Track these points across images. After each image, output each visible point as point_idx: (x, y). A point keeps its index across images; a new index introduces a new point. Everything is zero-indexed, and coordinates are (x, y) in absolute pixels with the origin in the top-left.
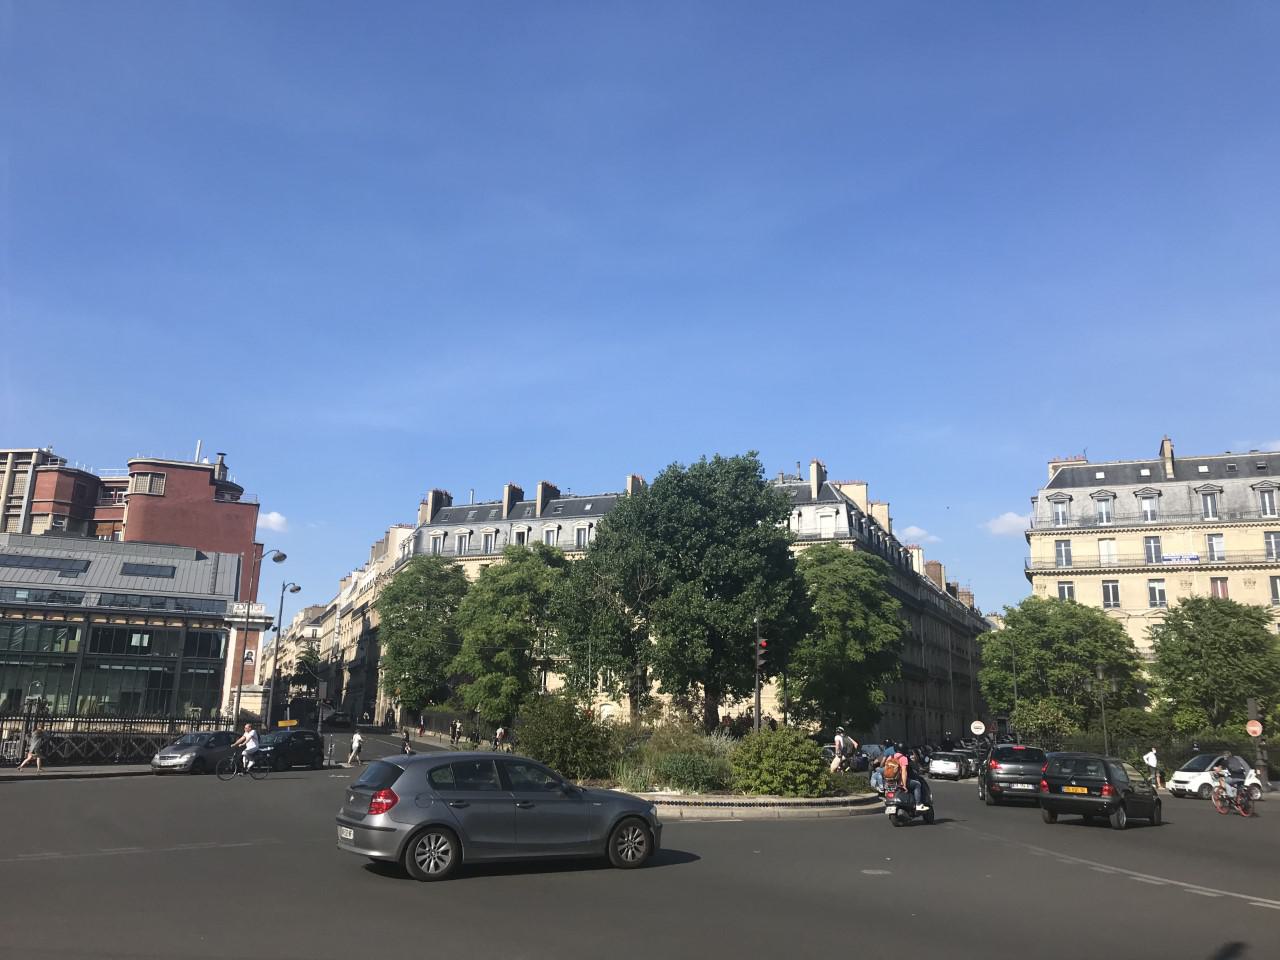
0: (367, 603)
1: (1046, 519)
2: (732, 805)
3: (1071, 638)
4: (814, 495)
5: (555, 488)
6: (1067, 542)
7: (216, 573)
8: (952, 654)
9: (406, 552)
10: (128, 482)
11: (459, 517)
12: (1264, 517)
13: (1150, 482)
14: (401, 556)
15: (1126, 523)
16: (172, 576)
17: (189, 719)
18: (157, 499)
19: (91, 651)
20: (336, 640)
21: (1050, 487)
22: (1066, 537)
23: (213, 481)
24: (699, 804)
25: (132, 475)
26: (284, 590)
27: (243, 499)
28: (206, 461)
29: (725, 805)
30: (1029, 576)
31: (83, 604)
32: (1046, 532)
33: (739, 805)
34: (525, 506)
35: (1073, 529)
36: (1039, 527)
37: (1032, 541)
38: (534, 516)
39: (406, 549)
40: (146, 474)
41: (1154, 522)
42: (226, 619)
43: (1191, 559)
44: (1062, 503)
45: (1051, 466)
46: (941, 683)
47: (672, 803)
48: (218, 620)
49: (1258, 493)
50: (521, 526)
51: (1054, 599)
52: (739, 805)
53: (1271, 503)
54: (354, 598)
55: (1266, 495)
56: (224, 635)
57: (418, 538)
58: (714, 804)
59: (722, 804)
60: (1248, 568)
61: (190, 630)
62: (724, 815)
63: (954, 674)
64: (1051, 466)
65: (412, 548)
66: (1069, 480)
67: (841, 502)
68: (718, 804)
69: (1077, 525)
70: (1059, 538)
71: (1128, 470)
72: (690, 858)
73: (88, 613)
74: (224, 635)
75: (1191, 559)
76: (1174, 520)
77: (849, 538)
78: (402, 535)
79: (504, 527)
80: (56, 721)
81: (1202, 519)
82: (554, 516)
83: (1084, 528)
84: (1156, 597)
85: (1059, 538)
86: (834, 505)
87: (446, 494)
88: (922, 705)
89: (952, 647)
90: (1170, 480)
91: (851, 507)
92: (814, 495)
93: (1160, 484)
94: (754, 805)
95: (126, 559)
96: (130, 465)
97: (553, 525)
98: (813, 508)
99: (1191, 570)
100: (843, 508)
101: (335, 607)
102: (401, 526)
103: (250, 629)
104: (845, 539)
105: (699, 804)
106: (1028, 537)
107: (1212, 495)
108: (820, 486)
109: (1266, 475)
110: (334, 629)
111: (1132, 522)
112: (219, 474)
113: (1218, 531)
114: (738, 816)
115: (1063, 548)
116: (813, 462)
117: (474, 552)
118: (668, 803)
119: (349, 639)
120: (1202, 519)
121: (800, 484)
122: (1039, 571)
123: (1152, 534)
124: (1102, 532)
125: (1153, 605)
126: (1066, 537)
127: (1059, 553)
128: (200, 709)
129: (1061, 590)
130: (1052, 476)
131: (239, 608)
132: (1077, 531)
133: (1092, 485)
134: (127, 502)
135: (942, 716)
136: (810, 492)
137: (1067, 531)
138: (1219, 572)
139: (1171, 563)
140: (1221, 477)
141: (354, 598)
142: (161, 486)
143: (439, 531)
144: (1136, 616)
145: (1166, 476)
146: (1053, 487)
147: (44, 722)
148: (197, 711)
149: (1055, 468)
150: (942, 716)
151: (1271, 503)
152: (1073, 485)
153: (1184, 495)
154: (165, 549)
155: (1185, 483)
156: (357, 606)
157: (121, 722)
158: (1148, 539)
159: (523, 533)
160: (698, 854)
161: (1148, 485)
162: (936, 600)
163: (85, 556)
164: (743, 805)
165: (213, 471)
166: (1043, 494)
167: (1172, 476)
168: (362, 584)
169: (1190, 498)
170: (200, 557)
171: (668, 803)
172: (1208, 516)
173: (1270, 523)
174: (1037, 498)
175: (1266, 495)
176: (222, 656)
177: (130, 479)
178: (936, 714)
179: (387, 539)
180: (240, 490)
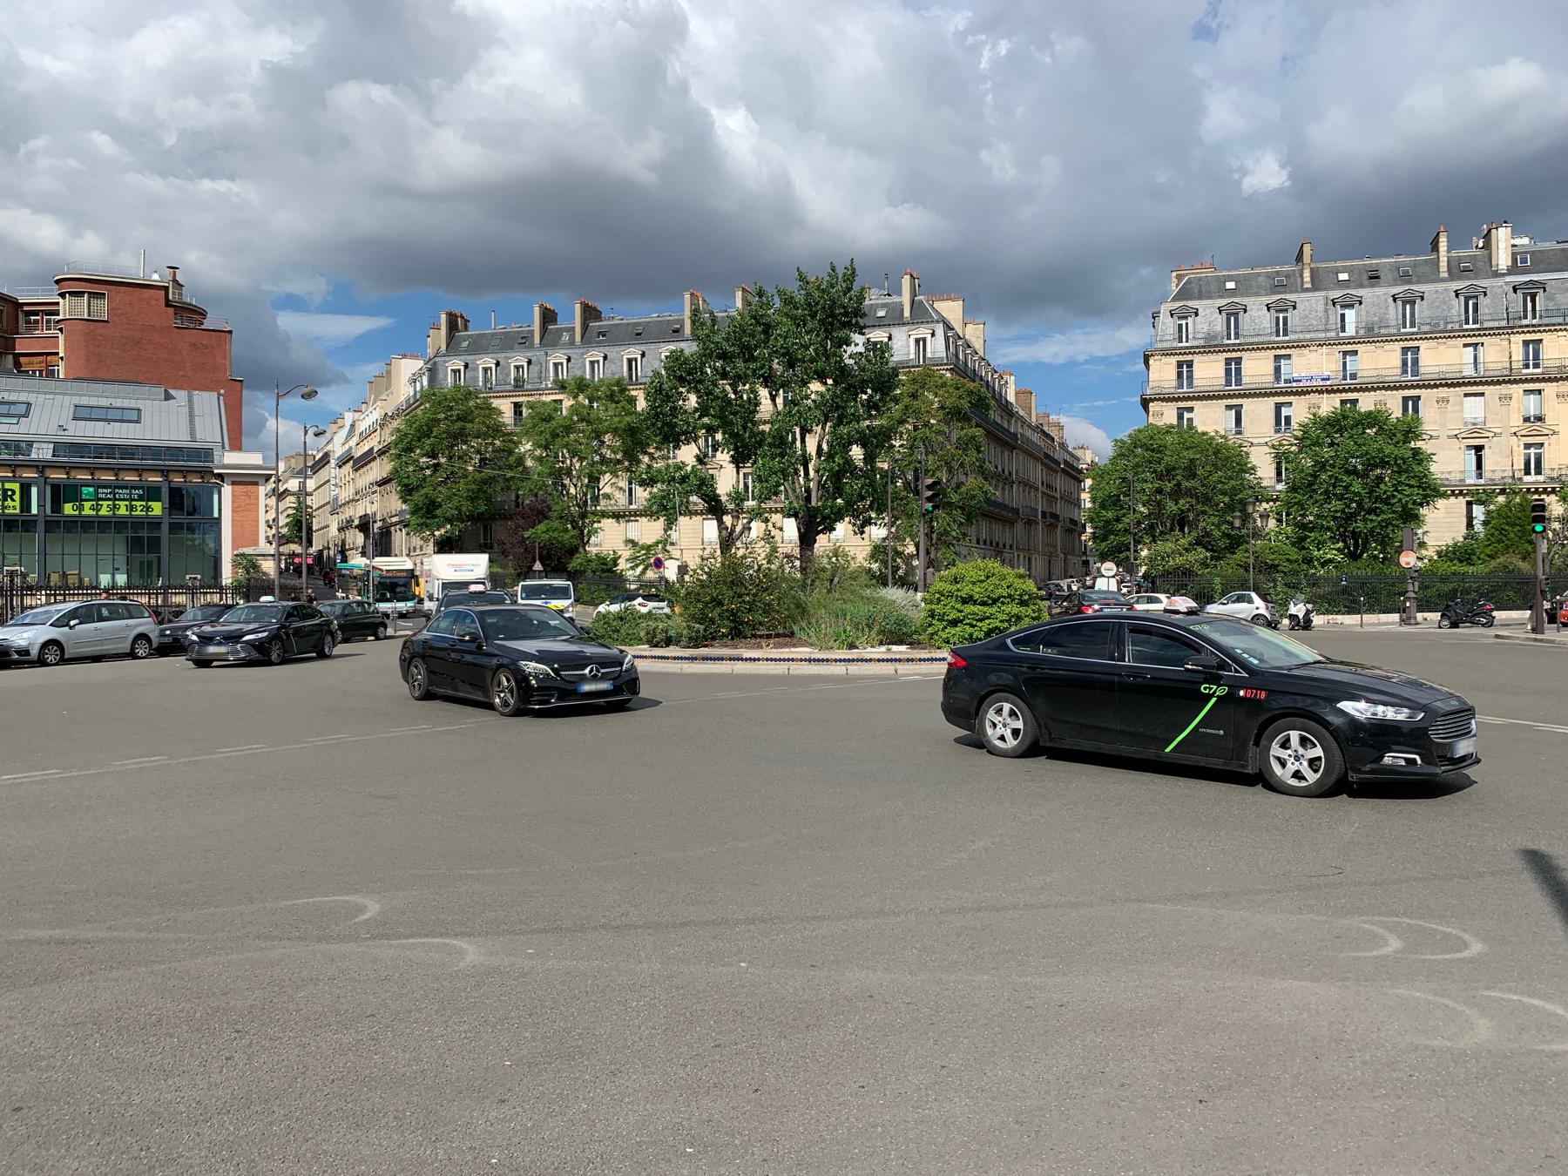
0: (372, 448)
3: (1191, 472)
4: (907, 314)
5: (595, 309)
7: (191, 415)
8: (1042, 492)
9: (418, 389)
10: (58, 304)
11: (479, 346)
12: (1403, 330)
13: (1348, 287)
14: (412, 394)
15: (1256, 340)
16: (138, 422)
17: (188, 588)
18: (101, 324)
19: (52, 512)
20: (333, 493)
21: (1174, 300)
23: (168, 303)
24: (912, 660)
25: (62, 295)
26: (305, 434)
27: (207, 324)
28: (156, 277)
30: (1145, 403)
31: (34, 456)
34: (561, 331)
35: (1197, 347)
36: (1159, 345)
37: (1151, 362)
38: (572, 343)
39: (418, 384)
40: (81, 294)
41: (1286, 338)
42: (216, 471)
43: (1323, 379)
44: (1352, 306)
45: (1174, 274)
48: (206, 473)
49: (1399, 303)
53: (1413, 314)
54: (352, 443)
55: (1408, 306)
56: (216, 491)
57: (433, 372)
58: (928, 660)
59: (936, 660)
60: (1314, 392)
61: (172, 485)
63: (1042, 512)
64: (1174, 274)
65: (425, 383)
67: (937, 322)
68: (932, 660)
69: (1202, 342)
70: (1181, 358)
71: (1261, 279)
73: (41, 467)
74: (216, 491)
75: (1323, 379)
76: (1308, 336)
77: (946, 364)
78: (408, 367)
80: (27, 595)
81: (1461, 325)
83: (1210, 346)
84: (1281, 421)
85: (1181, 358)
86: (887, 329)
90: (1307, 290)
91: (948, 327)
92: (907, 314)
95: (77, 400)
96: (57, 282)
98: (906, 328)
99: (1321, 392)
101: (326, 455)
103: (247, 480)
104: (942, 365)
105: (912, 660)
107: (1413, 303)
108: (913, 302)
109: (1410, 282)
110: (328, 481)
111: (1261, 339)
112: (174, 293)
113: (1354, 347)
116: (906, 274)
118: (879, 660)
119: (352, 491)
120: (1461, 325)
122: (1157, 397)
123: (1411, 344)
124: (1229, 350)
125: (1277, 431)
126: (1189, 357)
128: (199, 577)
130: (1175, 289)
131: (231, 458)
132: (1202, 350)
133: (1221, 297)
134: (61, 330)
135: (1029, 559)
137: (1192, 350)
138: (1349, 394)
139: (1301, 384)
140: (1362, 286)
141: (352, 443)
142: (102, 308)
143: (457, 363)
144: (1259, 445)
145: (1302, 285)
146: (1180, 300)
147: (157, 594)
148: (195, 578)
150: (1029, 559)
151: (1413, 314)
152: (1200, 297)
153: (1321, 308)
154: (116, 387)
155: (1323, 293)
156: (358, 453)
157: (145, 594)
159: (459, 371)
161: (1283, 296)
162: (1028, 433)
163: (23, 397)
165: (166, 289)
166: (1164, 309)
167: (1309, 286)
168: (362, 427)
169: (1326, 312)
170: (168, 397)
171: (879, 660)
172: (1405, 327)
173: (1408, 337)
174: (1159, 312)
175: (1408, 306)
176: (216, 515)
177: (61, 300)
178: (1019, 556)
179: (389, 372)
180: (203, 314)
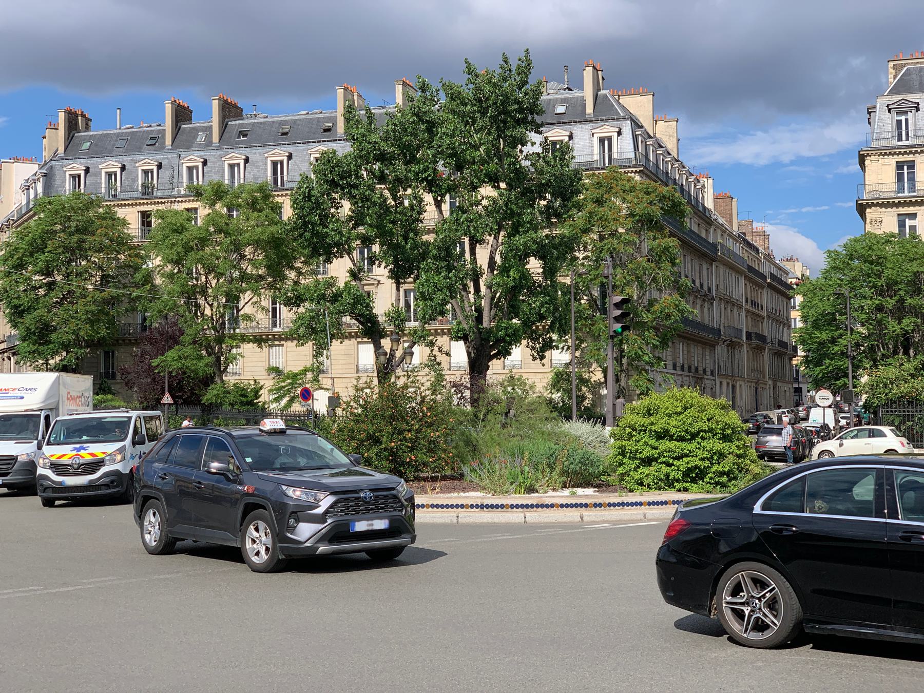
1: (885, 135)
2: (641, 504)
4: (589, 110)
6: (911, 165)
8: (748, 311)
9: (32, 196)
11: (101, 149)
21: (891, 93)
22: (910, 158)
24: (600, 505)
29: (632, 504)
30: (862, 209)
32: (885, 152)
33: (649, 504)
34: (195, 131)
38: (208, 144)
39: (32, 191)
45: (891, 64)
46: (732, 345)
47: (567, 506)
50: (193, 159)
51: (892, 235)
52: (649, 504)
57: (48, 177)
58: (619, 504)
59: (628, 504)
62: (634, 517)
66: (917, 83)
67: (624, 119)
72: (442, 554)
77: (634, 166)
79: (166, 158)
82: (237, 143)
85: (901, 158)
86: (567, 127)
87: (83, 115)
88: (712, 373)
89: (747, 301)
91: (636, 124)
92: (589, 110)
93: (918, 95)
94: (641, 504)
97: (237, 157)
98: (588, 126)
100: (627, 127)
102: (16, 160)
104: (630, 167)
106: (862, 162)
108: (596, 97)
114: (651, 517)
115: (906, 171)
117: (129, 195)
118: (562, 506)
121: (567, 96)
126: (910, 158)
127: (900, 177)
129: (902, 225)
135: (733, 387)
136: (584, 106)
143: (77, 167)
149: (897, 68)
150: (733, 387)
158: (900, 166)
159: (79, 176)
160: (444, 550)
162: (730, 243)
164: (654, 503)
166: (881, 103)
171: (562, 506)
174: (875, 107)
178: (728, 384)
